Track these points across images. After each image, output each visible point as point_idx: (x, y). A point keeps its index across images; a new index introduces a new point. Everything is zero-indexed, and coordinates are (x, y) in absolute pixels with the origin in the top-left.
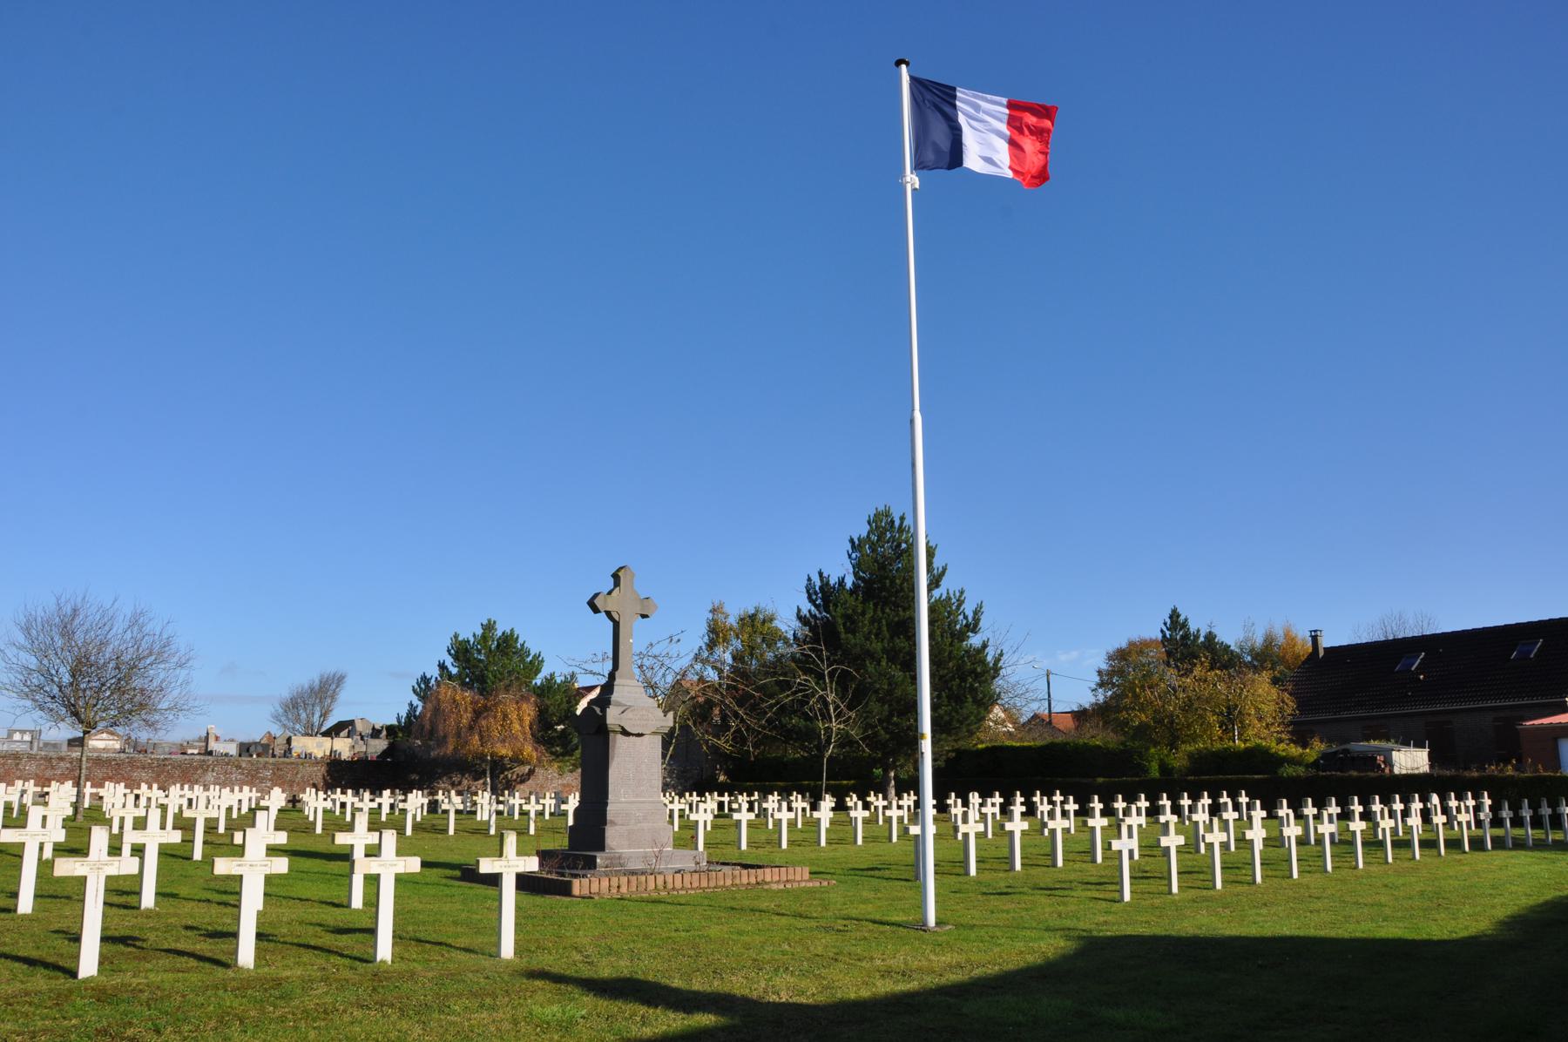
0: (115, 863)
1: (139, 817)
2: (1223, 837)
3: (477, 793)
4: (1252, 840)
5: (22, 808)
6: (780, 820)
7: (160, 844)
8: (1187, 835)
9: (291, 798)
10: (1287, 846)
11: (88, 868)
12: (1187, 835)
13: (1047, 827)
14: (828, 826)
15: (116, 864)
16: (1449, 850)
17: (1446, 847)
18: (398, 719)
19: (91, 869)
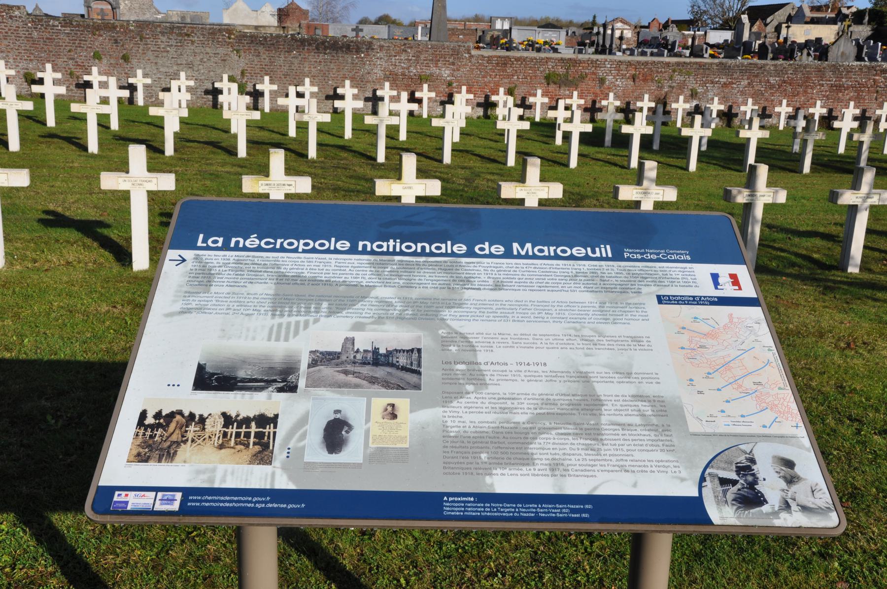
0: (153, 179)
1: (769, 204)
2: (525, 404)
3: (713, 99)
4: (647, 124)
5: (392, 133)
6: (570, 133)
7: (655, 202)
8: (794, 192)
9: (482, 100)
10: (271, 448)
11: (130, 183)
12: (794, 192)
13: (713, 129)
14: (457, 139)
15: (155, 180)
16: (704, 165)
17: (699, 160)
18: (238, 416)
19: (133, 184)
